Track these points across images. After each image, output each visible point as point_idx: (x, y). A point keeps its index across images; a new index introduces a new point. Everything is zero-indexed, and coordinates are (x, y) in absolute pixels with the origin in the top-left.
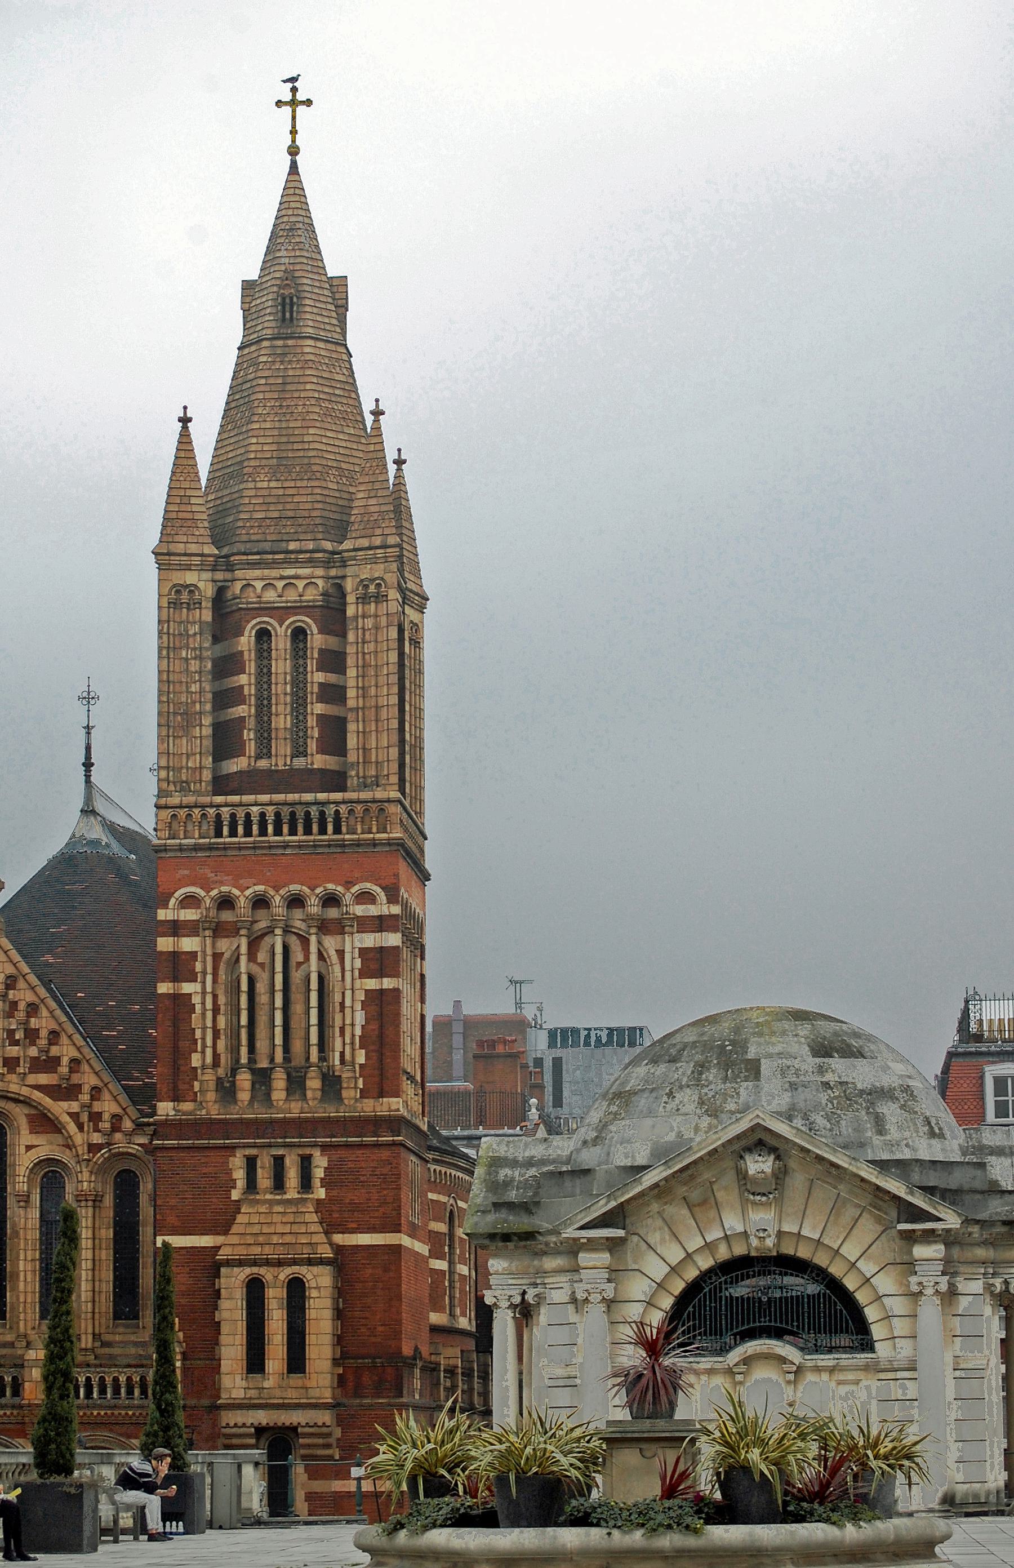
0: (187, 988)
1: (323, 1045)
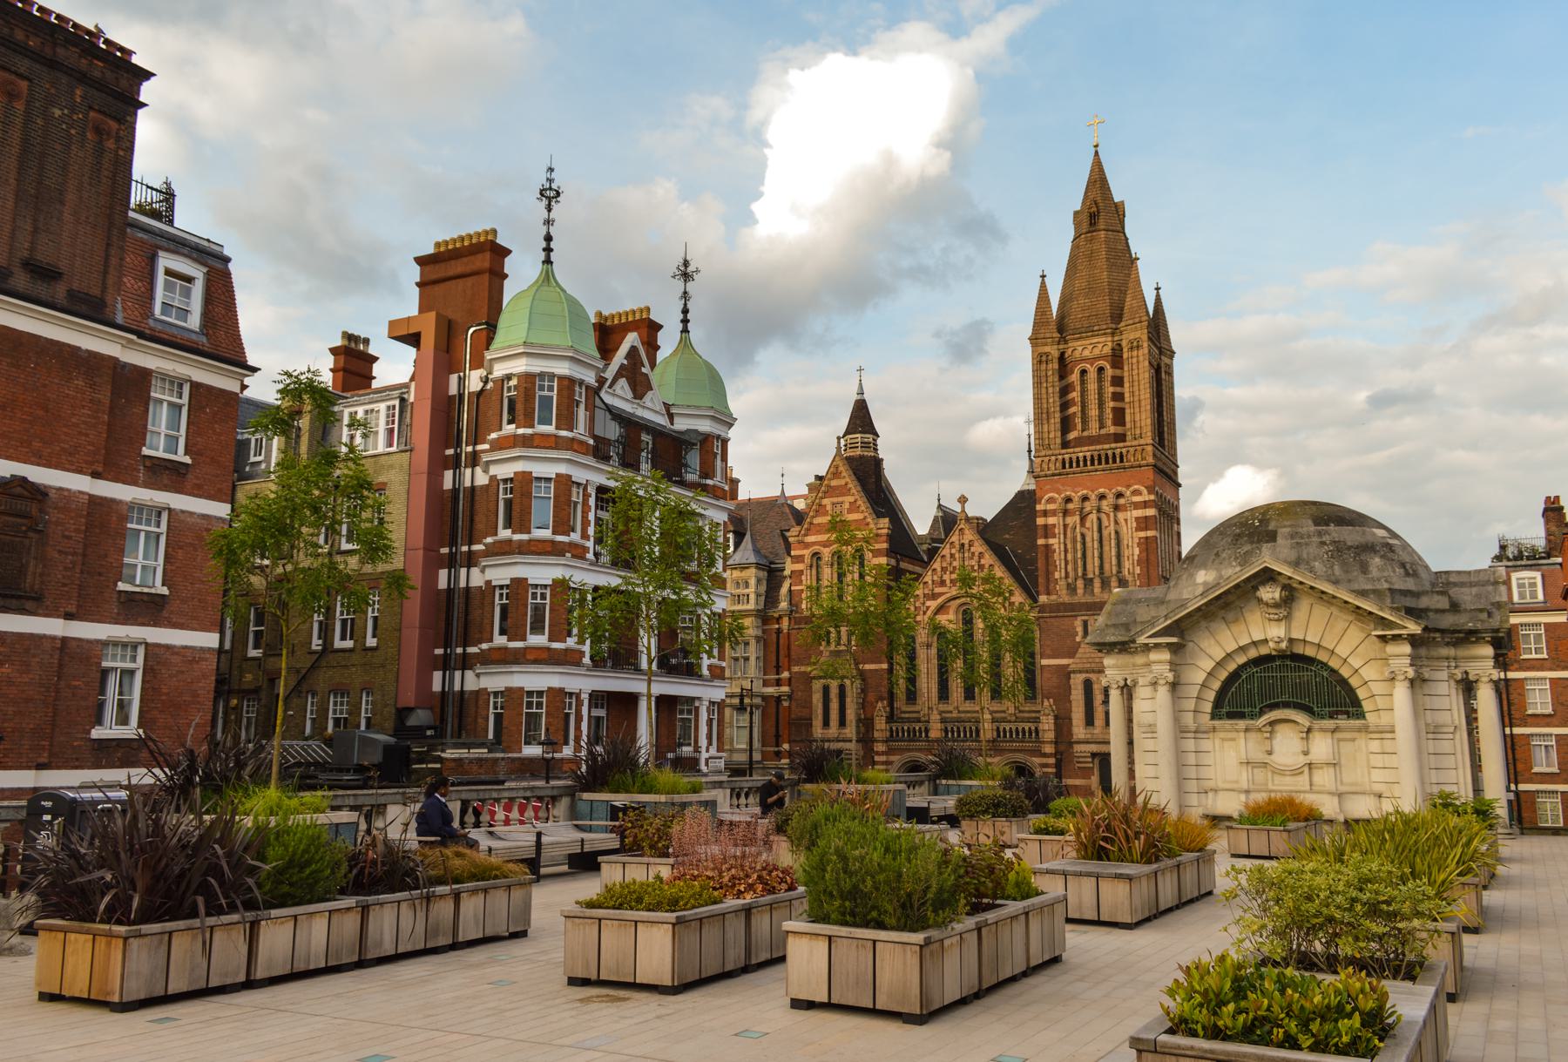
0: (1051, 541)
1: (1119, 564)
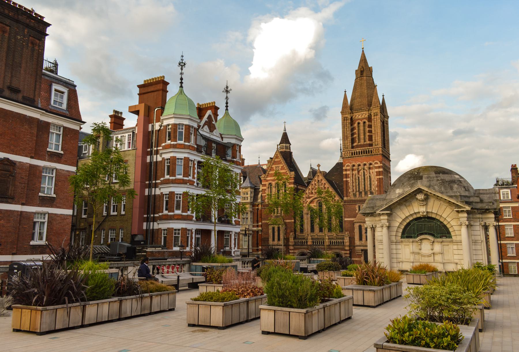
0: (348, 179)
1: (370, 187)
